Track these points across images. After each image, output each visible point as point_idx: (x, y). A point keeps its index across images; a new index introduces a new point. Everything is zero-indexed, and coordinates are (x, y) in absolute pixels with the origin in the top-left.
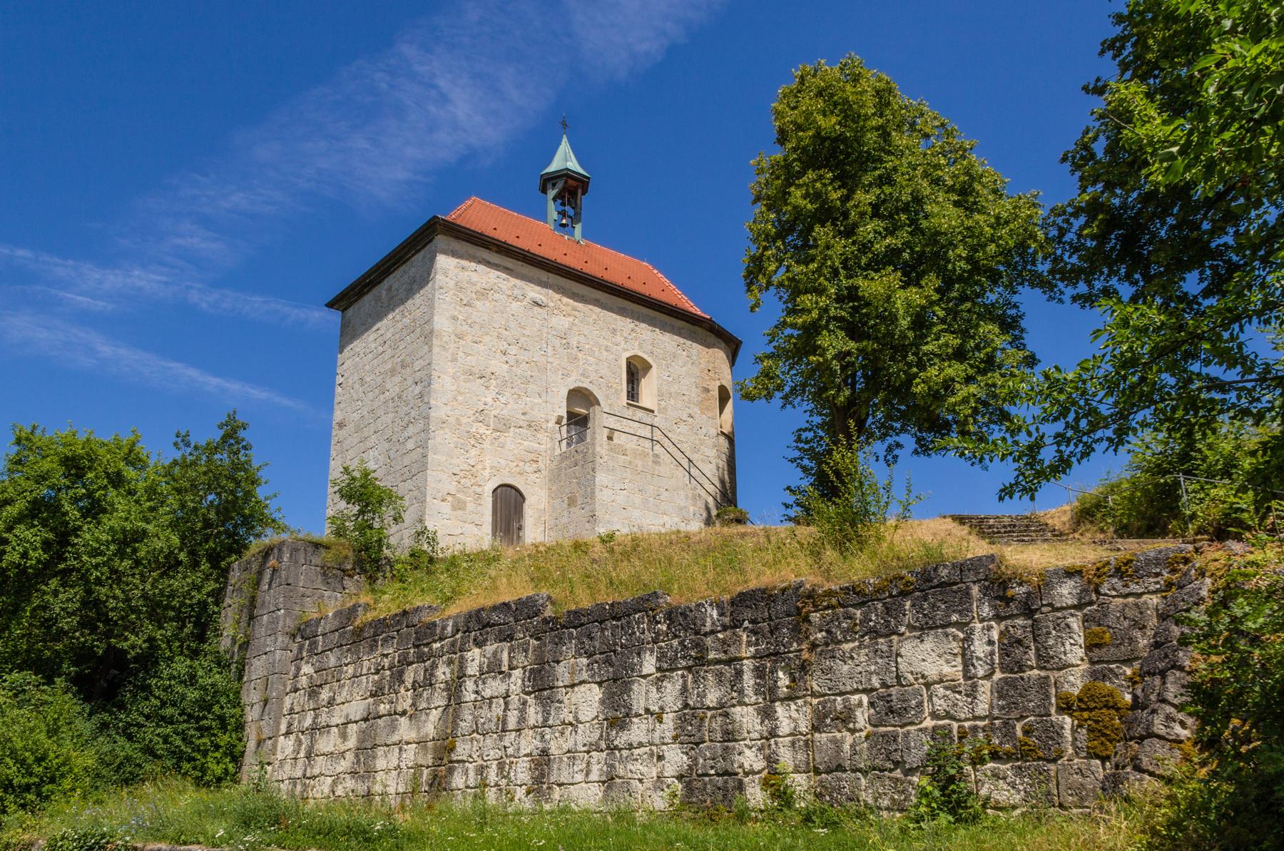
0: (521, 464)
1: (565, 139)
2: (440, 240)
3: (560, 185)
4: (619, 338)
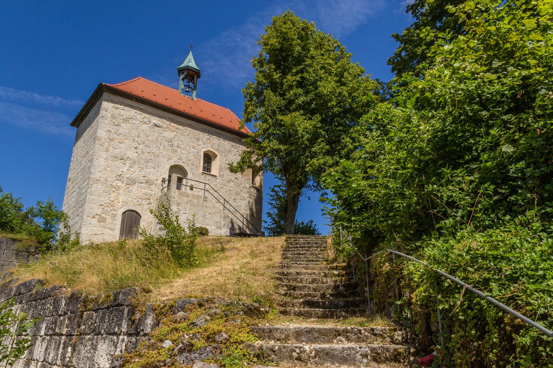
0: (140, 200)
1: (191, 53)
2: (105, 95)
3: (186, 73)
4: (200, 142)
